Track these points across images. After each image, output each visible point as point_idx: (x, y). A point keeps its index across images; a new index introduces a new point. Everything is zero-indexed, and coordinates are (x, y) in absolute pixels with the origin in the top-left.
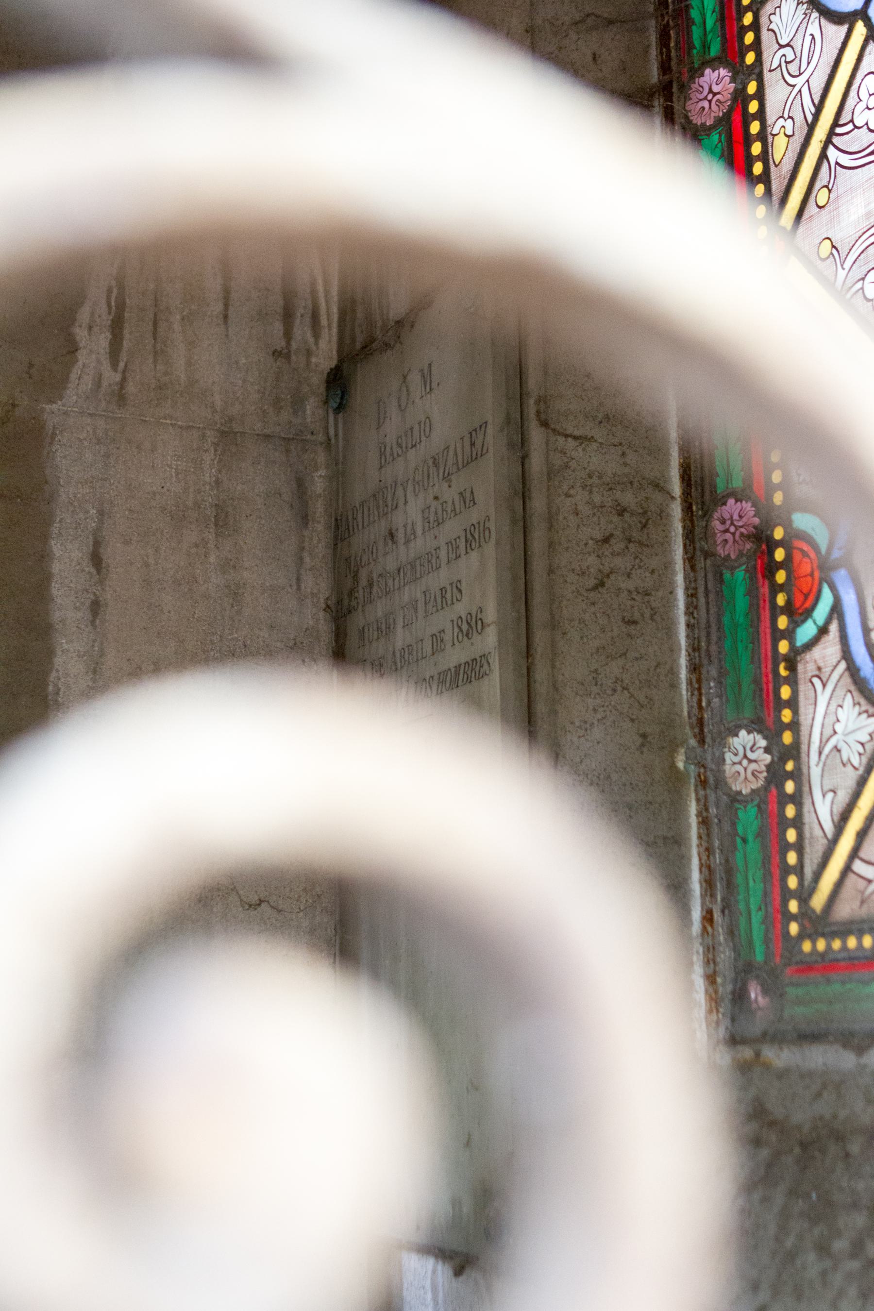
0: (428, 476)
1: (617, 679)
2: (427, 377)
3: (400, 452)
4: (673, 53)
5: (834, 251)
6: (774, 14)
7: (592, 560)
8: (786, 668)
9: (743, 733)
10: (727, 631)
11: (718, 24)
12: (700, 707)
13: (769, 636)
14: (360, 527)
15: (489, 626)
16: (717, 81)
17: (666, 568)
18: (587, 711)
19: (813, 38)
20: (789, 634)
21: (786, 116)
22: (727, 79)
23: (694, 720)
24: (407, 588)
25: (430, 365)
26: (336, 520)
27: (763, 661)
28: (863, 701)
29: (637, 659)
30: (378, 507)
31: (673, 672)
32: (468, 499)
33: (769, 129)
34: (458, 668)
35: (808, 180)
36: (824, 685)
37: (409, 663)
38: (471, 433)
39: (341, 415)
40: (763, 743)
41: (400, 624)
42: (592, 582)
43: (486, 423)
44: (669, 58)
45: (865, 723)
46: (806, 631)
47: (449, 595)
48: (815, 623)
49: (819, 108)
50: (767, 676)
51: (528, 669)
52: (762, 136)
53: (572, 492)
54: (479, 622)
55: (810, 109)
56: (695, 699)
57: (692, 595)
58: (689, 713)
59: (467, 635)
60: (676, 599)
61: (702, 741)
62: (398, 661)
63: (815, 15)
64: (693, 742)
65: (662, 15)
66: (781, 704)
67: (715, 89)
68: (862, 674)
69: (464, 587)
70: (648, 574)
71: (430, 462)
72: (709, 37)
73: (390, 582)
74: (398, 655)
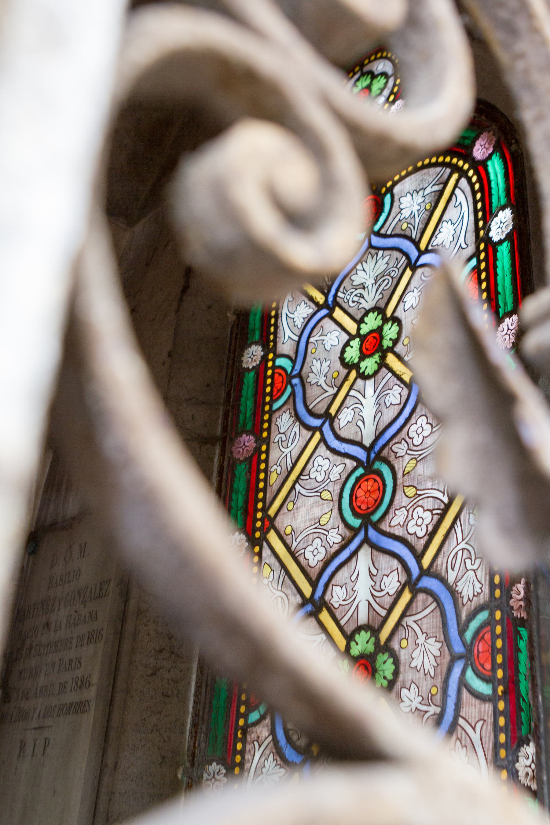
0: (74, 599)
1: (155, 725)
2: (83, 549)
3: (61, 583)
4: (229, 423)
5: (293, 532)
6: (348, 422)
7: (152, 660)
8: (241, 734)
9: (214, 764)
10: (214, 708)
11: (252, 416)
12: (194, 746)
13: (235, 716)
14: (31, 616)
15: (93, 685)
16: (248, 441)
17: (188, 670)
18: (137, 740)
19: (296, 433)
20: (245, 716)
21: (278, 464)
22: (253, 441)
23: (190, 753)
24: (51, 655)
25: (85, 544)
26: (18, 610)
27: (230, 728)
28: (278, 759)
29: (166, 716)
30: (43, 608)
31: (183, 725)
32: (93, 616)
33: (269, 469)
34: (71, 704)
35: (285, 496)
36: (259, 747)
37: (44, 696)
38: (101, 584)
39: (32, 557)
40: (224, 771)
41: (43, 674)
42: (150, 672)
43: (110, 580)
44: (227, 425)
45: (278, 771)
46: (254, 716)
47: (73, 665)
48: (259, 713)
49: (294, 465)
50: (231, 736)
51: (109, 712)
52: (266, 471)
53: (148, 623)
54: (88, 683)
55: (290, 464)
56: (192, 742)
57: (199, 687)
58: (188, 749)
59: (80, 688)
60: (190, 687)
61: (193, 765)
62: (38, 693)
63: (298, 423)
64: (188, 764)
65: (227, 406)
66: (236, 752)
67: (247, 444)
68: (280, 744)
69: (82, 662)
70: (178, 672)
71: (76, 593)
72: (247, 421)
73: (42, 650)
74: (39, 690)
